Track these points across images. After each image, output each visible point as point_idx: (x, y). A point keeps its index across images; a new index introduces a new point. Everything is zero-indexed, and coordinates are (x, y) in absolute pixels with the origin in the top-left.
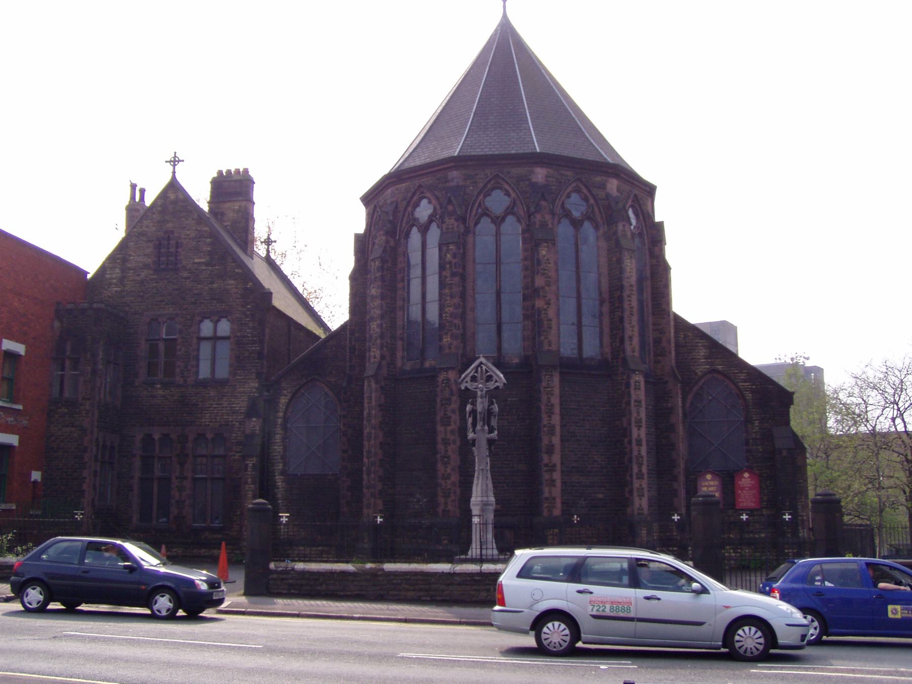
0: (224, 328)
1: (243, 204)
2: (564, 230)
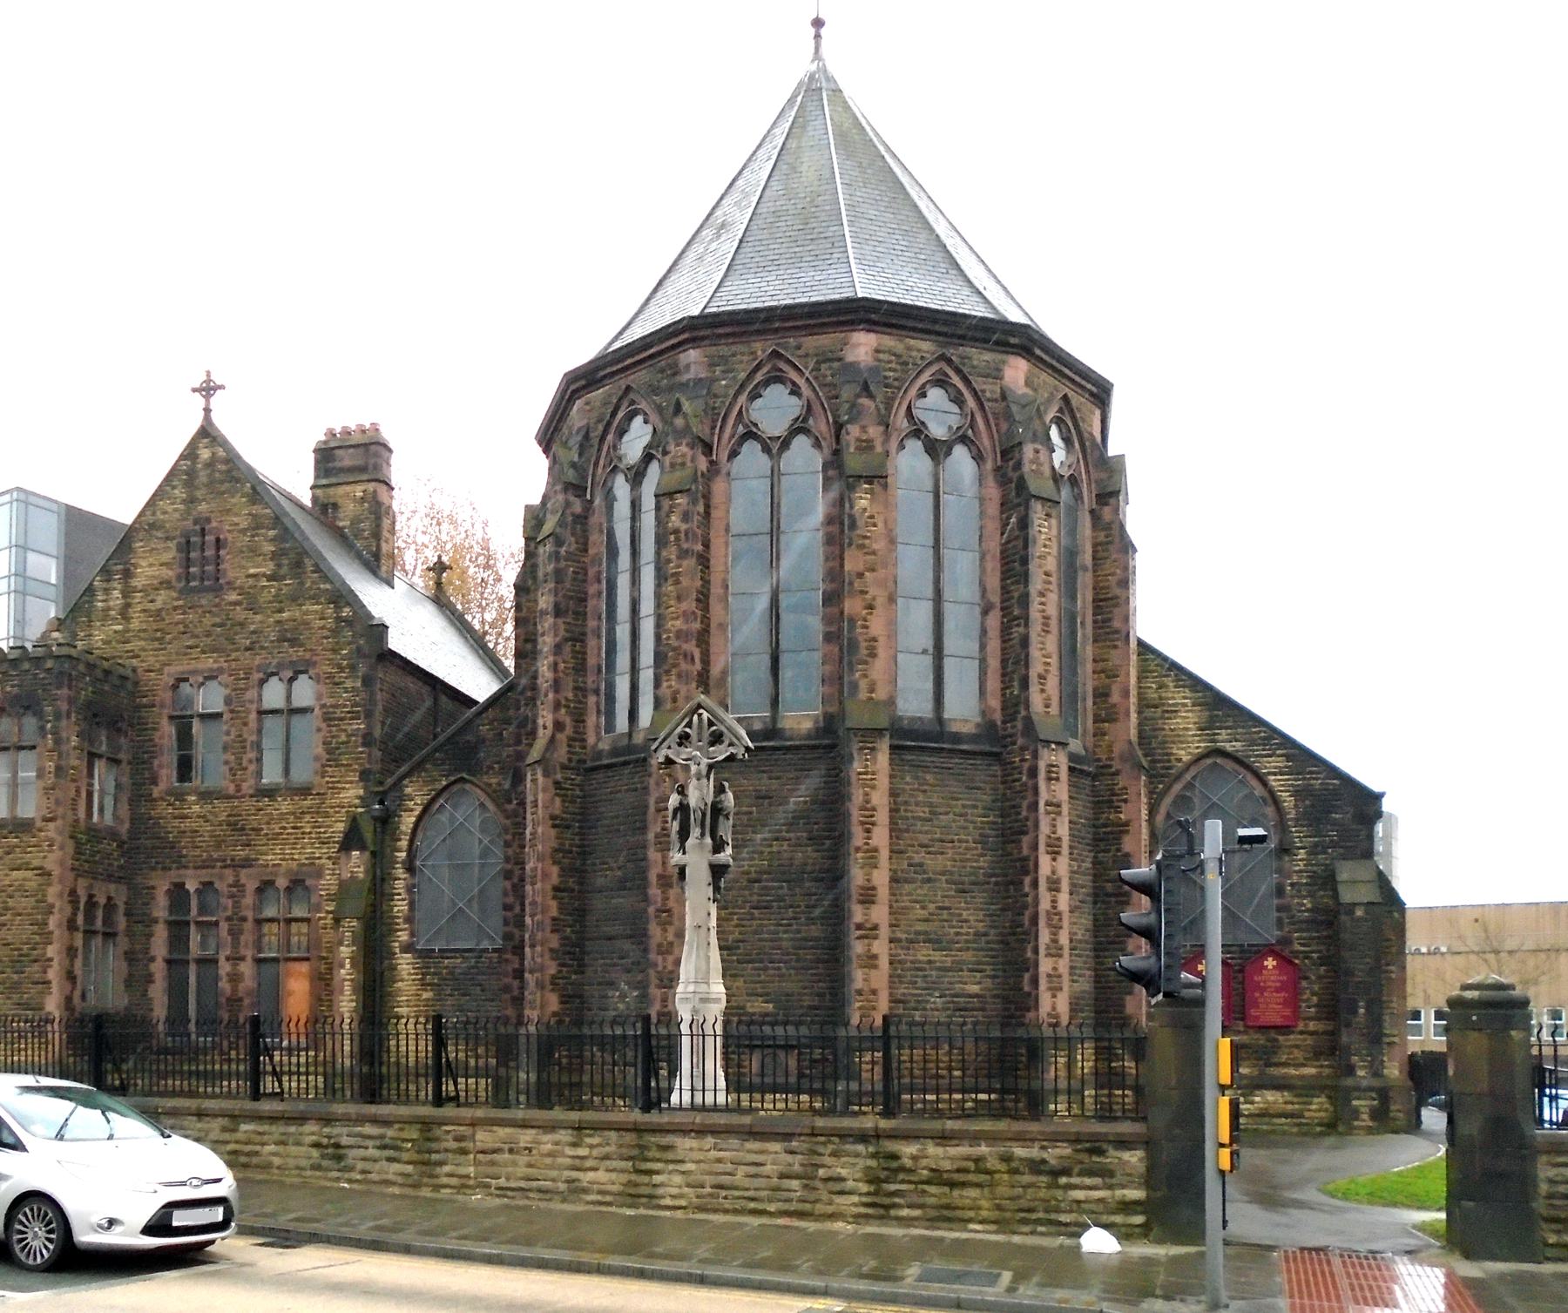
0: (305, 694)
1: (371, 487)
2: (910, 463)
